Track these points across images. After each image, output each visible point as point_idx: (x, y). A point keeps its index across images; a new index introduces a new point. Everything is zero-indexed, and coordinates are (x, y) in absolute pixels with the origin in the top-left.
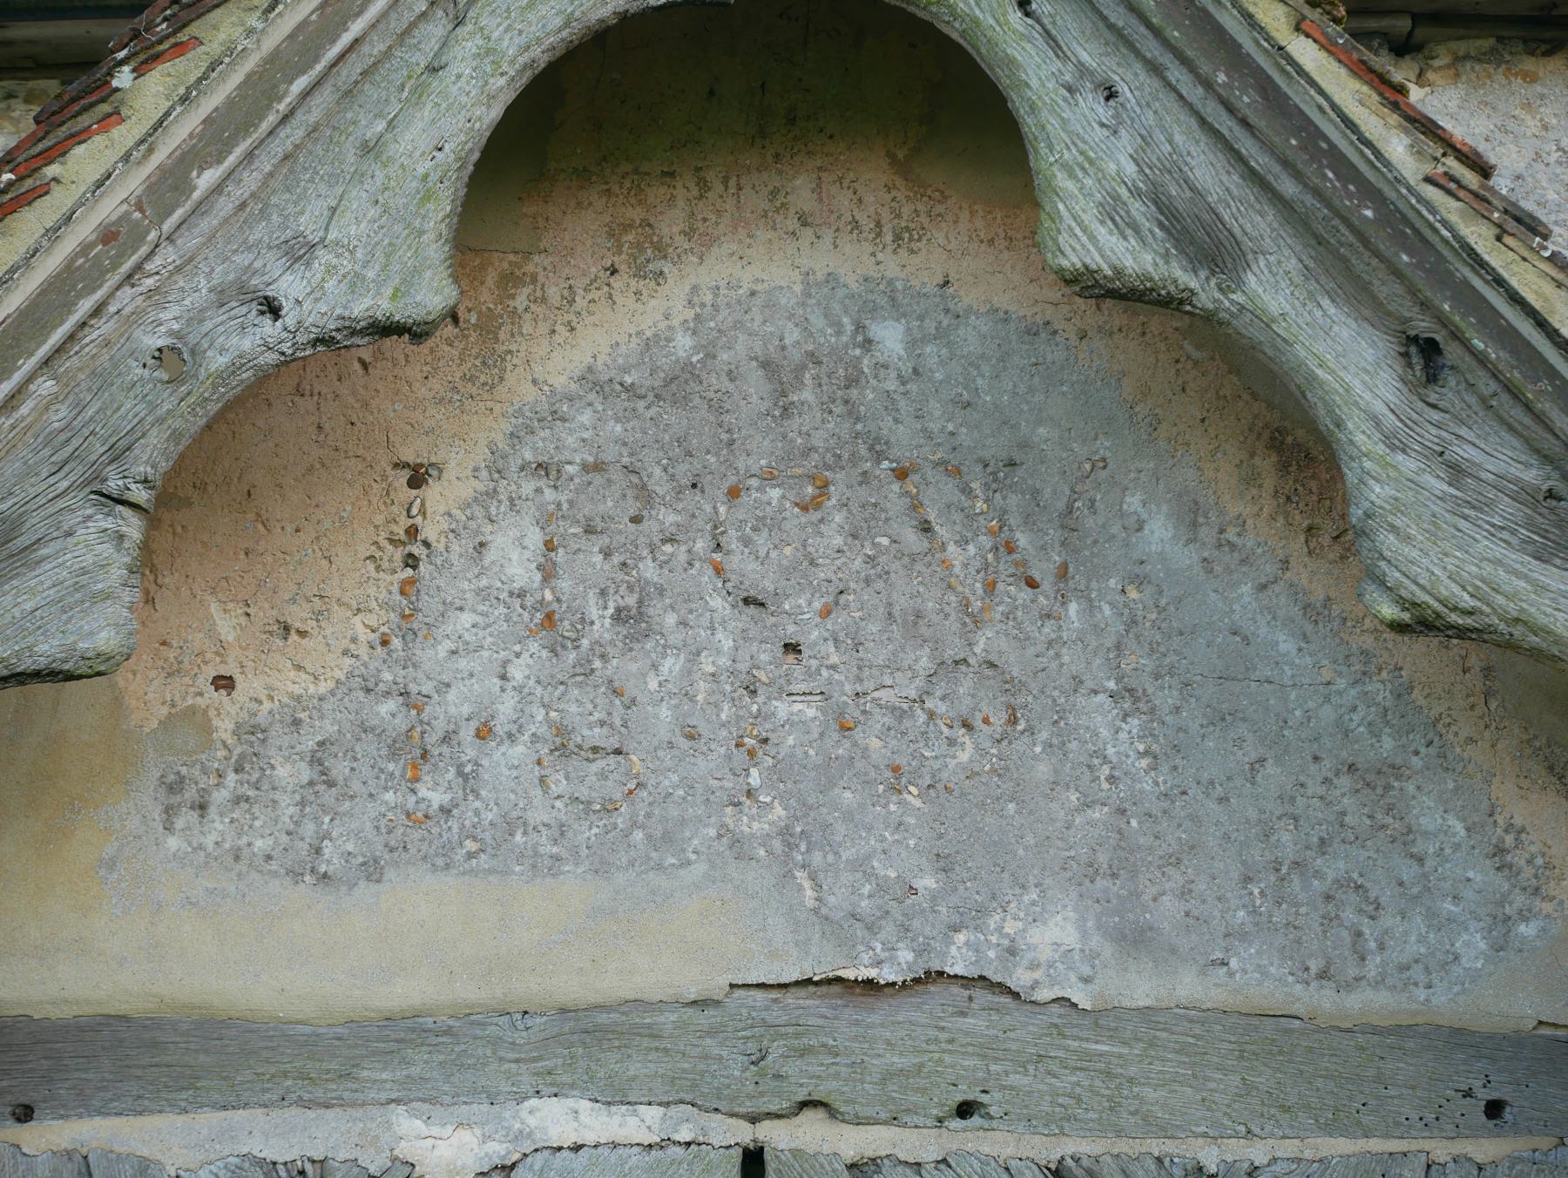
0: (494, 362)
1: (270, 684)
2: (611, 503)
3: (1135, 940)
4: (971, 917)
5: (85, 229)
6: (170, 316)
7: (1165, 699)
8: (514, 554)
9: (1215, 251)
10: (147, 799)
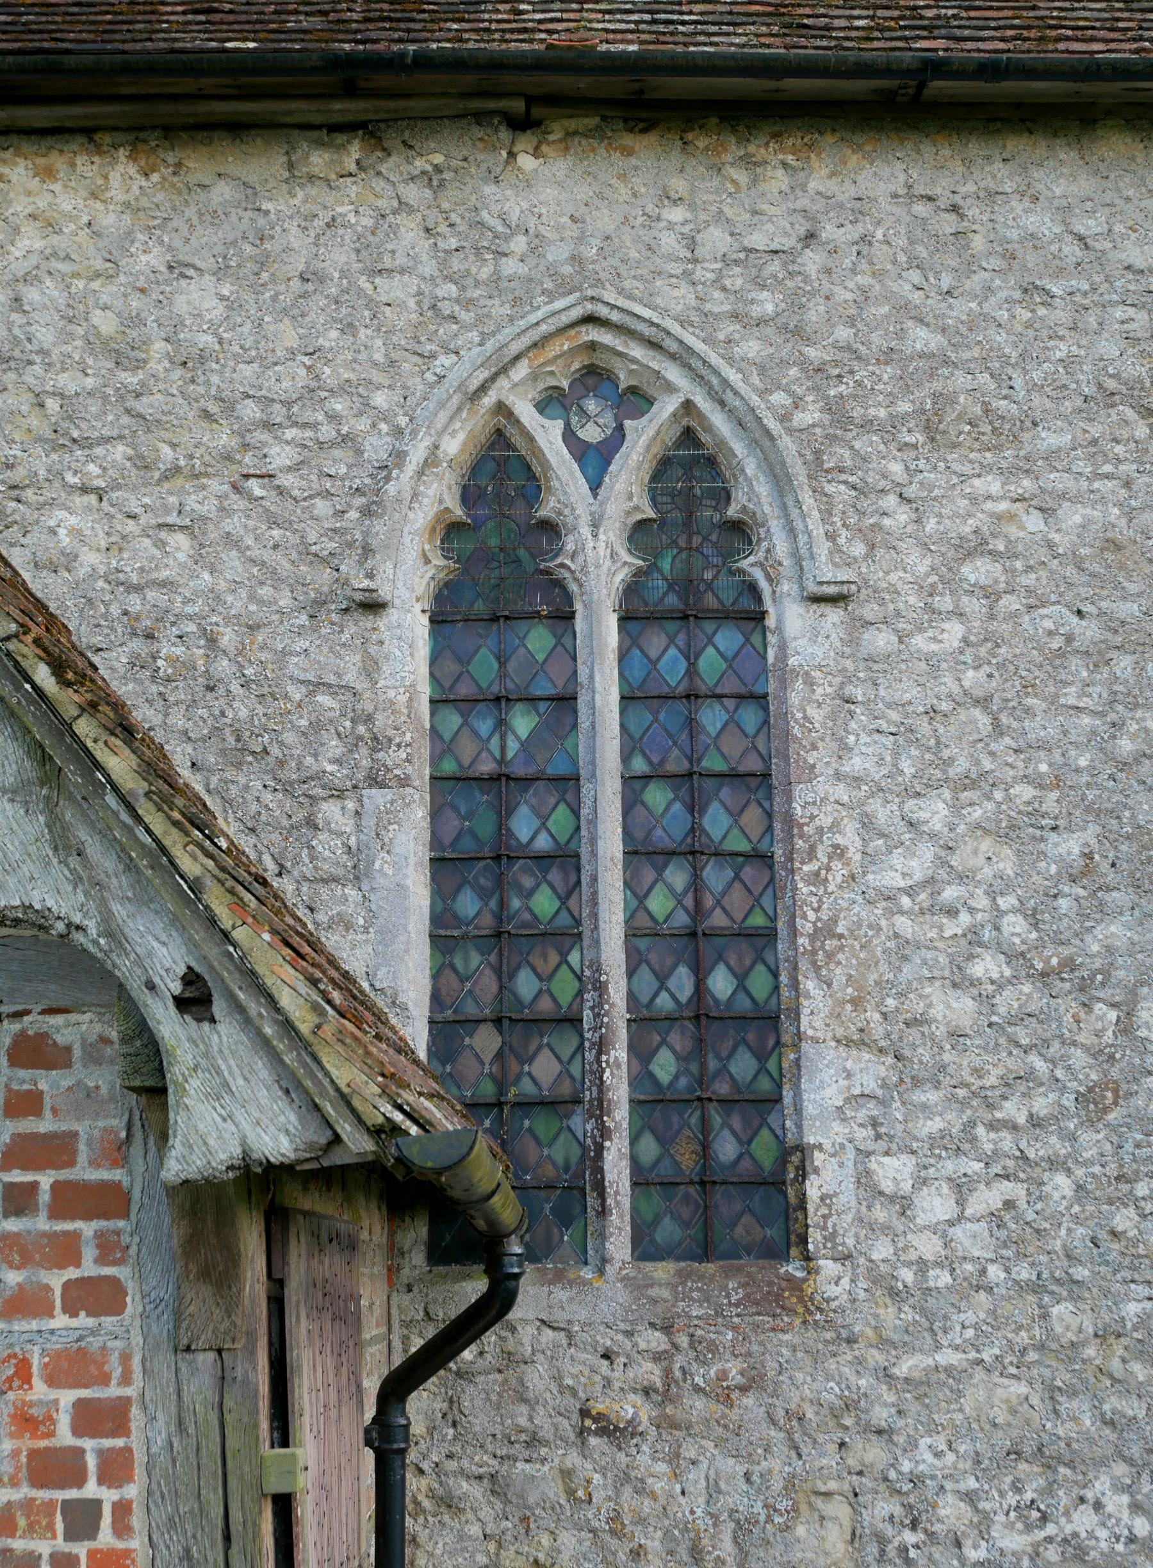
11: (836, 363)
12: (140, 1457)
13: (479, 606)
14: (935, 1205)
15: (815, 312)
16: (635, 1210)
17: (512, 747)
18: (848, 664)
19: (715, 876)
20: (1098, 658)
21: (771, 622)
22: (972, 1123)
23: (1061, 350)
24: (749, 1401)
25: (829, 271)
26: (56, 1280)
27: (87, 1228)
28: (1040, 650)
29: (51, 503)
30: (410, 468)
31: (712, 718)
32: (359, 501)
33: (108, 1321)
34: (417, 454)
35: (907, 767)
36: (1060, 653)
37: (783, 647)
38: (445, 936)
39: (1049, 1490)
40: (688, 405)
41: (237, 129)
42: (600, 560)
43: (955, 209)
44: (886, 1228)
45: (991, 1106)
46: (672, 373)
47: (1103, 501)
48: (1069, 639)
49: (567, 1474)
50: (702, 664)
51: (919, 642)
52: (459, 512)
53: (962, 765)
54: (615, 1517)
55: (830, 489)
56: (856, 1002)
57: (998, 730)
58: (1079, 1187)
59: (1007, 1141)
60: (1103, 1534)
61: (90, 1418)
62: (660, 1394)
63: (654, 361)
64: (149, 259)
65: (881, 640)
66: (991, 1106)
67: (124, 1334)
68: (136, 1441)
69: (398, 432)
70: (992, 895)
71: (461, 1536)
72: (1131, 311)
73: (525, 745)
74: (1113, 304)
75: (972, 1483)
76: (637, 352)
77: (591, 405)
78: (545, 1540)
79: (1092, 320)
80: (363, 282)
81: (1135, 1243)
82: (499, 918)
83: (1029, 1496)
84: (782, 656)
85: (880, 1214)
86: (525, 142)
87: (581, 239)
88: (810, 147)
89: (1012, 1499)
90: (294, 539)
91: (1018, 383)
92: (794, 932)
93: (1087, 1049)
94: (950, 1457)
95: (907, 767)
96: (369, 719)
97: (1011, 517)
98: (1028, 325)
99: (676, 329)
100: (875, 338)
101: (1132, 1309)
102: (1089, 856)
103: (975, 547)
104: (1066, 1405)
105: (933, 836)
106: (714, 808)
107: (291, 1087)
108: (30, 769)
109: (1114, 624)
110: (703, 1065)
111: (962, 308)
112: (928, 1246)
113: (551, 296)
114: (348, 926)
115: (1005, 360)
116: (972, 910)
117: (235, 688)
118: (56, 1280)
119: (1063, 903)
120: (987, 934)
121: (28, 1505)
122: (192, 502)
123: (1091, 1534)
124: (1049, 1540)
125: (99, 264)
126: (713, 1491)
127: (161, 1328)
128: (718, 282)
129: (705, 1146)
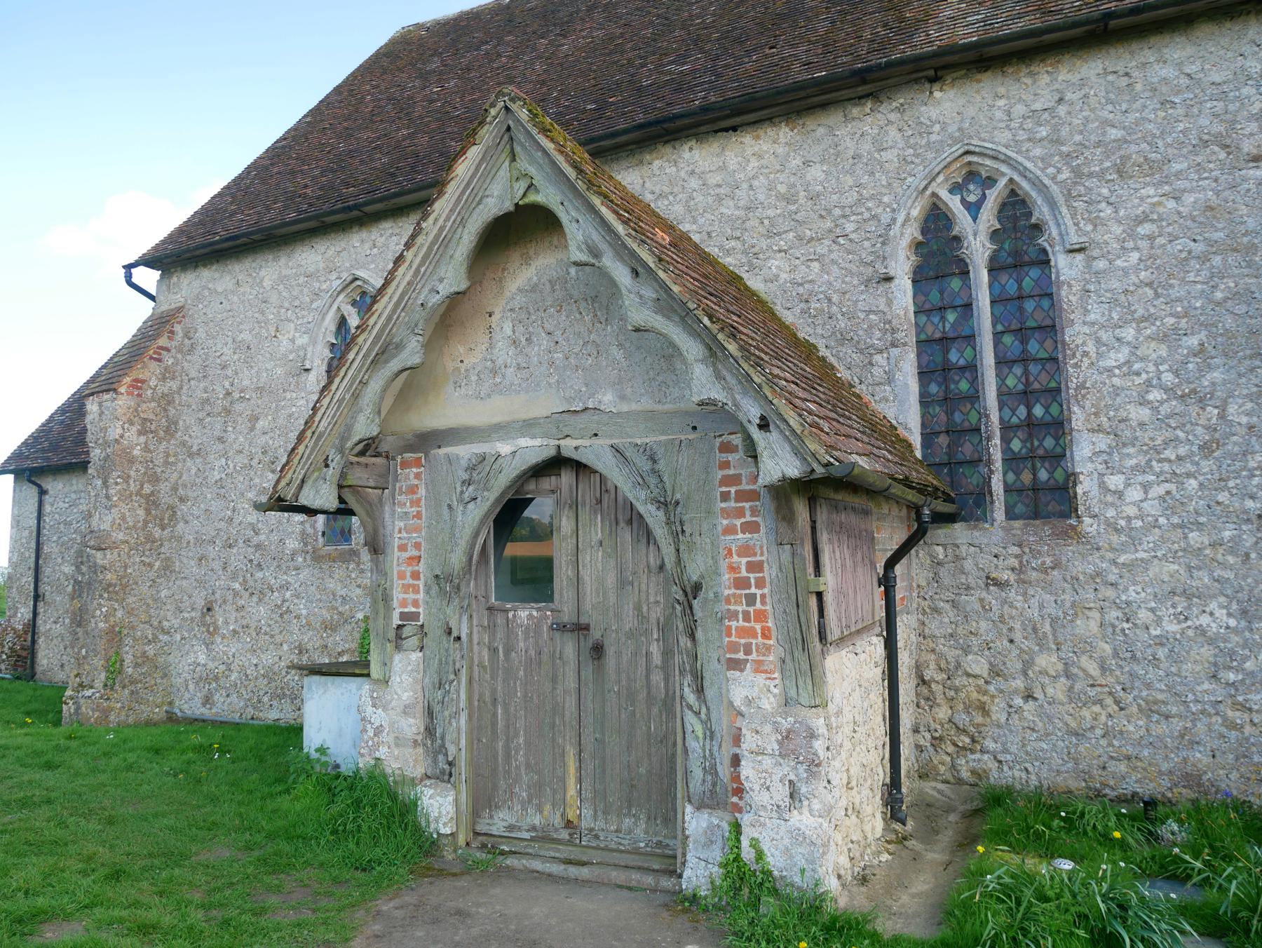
0: (502, 288)
1: (471, 360)
2: (524, 316)
3: (623, 397)
4: (592, 396)
5: (405, 283)
6: (422, 297)
7: (628, 345)
8: (508, 330)
9: (596, 253)
10: (451, 386)
11: (1075, 151)
12: (768, 580)
13: (931, 273)
14: (1135, 494)
15: (1065, 131)
16: (1006, 501)
17: (948, 326)
18: (1087, 276)
19: (1034, 369)
20: (1204, 258)
21: (1052, 263)
22: (1150, 460)
23: (1181, 126)
24: (1055, 573)
25: (1070, 113)
26: (738, 522)
27: (747, 505)
28: (1176, 259)
29: (769, 258)
30: (899, 224)
31: (1029, 305)
32: (881, 240)
33: (755, 535)
34: (901, 218)
35: (1115, 316)
36: (1186, 259)
37: (1058, 273)
38: (925, 401)
39: (1189, 607)
40: (1011, 180)
41: (824, 106)
42: (978, 247)
43: (1127, 74)
44: (1112, 504)
45: (1159, 453)
46: (1004, 168)
47: (1204, 189)
48: (1190, 252)
49: (982, 600)
50: (1024, 284)
51: (1119, 263)
52: (920, 238)
53: (1140, 312)
54: (1002, 616)
55: (1075, 204)
56: (1096, 414)
57: (1157, 295)
58: (1201, 484)
59: (1166, 467)
60: (1214, 625)
61: (752, 567)
62: (1019, 570)
63: (995, 165)
64: (796, 162)
65: (1101, 264)
66: (1159, 453)
67: (761, 539)
68: (766, 574)
69: (894, 210)
70: (1156, 365)
71: (941, 622)
72: (1215, 103)
73: (953, 325)
74: (1205, 101)
75: (1153, 605)
76: (988, 162)
77: (971, 187)
78: (974, 624)
79: (1195, 110)
80: (876, 155)
81: (1228, 506)
82: (945, 392)
83: (1179, 610)
84: (1058, 277)
85: (1110, 499)
86: (936, 86)
87: (962, 121)
88: (1058, 62)
89: (1172, 611)
90: (857, 258)
91: (1160, 144)
92: (1068, 388)
93: (1203, 426)
94: (1143, 594)
95: (1115, 316)
96: (890, 322)
97: (1160, 203)
98: (1164, 118)
99: (1003, 150)
100: (1092, 137)
101: (1227, 534)
102: (1203, 345)
103: (1144, 219)
104: (1196, 573)
105: (1128, 343)
106: (1032, 342)
107: (797, 453)
108: (707, 353)
109: (1210, 243)
110: (1032, 444)
111: (1132, 117)
112: (1131, 511)
113: (951, 146)
114: (887, 401)
115: (1154, 136)
116: (1147, 372)
117: (839, 316)
118: (738, 522)
119: (1190, 366)
120: (1154, 382)
121: (734, 594)
122: (819, 250)
123: (1208, 625)
124: (1189, 627)
125: (778, 167)
126: (1041, 607)
127: (772, 538)
128: (1021, 127)
129: (1034, 475)
